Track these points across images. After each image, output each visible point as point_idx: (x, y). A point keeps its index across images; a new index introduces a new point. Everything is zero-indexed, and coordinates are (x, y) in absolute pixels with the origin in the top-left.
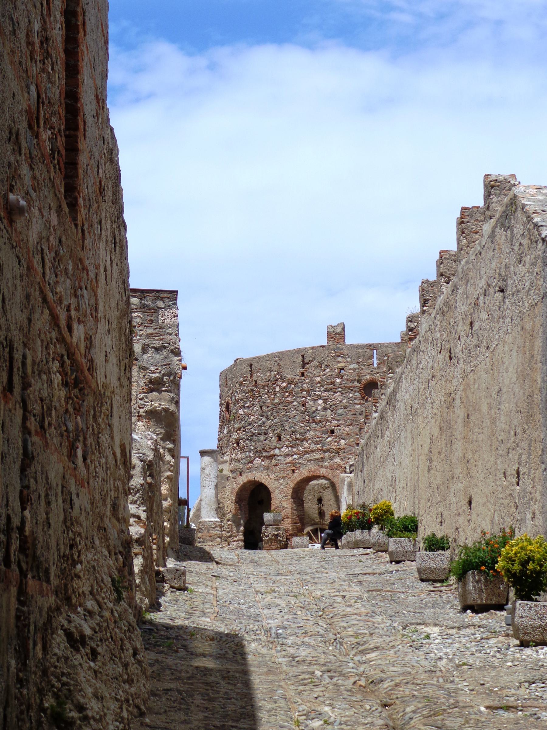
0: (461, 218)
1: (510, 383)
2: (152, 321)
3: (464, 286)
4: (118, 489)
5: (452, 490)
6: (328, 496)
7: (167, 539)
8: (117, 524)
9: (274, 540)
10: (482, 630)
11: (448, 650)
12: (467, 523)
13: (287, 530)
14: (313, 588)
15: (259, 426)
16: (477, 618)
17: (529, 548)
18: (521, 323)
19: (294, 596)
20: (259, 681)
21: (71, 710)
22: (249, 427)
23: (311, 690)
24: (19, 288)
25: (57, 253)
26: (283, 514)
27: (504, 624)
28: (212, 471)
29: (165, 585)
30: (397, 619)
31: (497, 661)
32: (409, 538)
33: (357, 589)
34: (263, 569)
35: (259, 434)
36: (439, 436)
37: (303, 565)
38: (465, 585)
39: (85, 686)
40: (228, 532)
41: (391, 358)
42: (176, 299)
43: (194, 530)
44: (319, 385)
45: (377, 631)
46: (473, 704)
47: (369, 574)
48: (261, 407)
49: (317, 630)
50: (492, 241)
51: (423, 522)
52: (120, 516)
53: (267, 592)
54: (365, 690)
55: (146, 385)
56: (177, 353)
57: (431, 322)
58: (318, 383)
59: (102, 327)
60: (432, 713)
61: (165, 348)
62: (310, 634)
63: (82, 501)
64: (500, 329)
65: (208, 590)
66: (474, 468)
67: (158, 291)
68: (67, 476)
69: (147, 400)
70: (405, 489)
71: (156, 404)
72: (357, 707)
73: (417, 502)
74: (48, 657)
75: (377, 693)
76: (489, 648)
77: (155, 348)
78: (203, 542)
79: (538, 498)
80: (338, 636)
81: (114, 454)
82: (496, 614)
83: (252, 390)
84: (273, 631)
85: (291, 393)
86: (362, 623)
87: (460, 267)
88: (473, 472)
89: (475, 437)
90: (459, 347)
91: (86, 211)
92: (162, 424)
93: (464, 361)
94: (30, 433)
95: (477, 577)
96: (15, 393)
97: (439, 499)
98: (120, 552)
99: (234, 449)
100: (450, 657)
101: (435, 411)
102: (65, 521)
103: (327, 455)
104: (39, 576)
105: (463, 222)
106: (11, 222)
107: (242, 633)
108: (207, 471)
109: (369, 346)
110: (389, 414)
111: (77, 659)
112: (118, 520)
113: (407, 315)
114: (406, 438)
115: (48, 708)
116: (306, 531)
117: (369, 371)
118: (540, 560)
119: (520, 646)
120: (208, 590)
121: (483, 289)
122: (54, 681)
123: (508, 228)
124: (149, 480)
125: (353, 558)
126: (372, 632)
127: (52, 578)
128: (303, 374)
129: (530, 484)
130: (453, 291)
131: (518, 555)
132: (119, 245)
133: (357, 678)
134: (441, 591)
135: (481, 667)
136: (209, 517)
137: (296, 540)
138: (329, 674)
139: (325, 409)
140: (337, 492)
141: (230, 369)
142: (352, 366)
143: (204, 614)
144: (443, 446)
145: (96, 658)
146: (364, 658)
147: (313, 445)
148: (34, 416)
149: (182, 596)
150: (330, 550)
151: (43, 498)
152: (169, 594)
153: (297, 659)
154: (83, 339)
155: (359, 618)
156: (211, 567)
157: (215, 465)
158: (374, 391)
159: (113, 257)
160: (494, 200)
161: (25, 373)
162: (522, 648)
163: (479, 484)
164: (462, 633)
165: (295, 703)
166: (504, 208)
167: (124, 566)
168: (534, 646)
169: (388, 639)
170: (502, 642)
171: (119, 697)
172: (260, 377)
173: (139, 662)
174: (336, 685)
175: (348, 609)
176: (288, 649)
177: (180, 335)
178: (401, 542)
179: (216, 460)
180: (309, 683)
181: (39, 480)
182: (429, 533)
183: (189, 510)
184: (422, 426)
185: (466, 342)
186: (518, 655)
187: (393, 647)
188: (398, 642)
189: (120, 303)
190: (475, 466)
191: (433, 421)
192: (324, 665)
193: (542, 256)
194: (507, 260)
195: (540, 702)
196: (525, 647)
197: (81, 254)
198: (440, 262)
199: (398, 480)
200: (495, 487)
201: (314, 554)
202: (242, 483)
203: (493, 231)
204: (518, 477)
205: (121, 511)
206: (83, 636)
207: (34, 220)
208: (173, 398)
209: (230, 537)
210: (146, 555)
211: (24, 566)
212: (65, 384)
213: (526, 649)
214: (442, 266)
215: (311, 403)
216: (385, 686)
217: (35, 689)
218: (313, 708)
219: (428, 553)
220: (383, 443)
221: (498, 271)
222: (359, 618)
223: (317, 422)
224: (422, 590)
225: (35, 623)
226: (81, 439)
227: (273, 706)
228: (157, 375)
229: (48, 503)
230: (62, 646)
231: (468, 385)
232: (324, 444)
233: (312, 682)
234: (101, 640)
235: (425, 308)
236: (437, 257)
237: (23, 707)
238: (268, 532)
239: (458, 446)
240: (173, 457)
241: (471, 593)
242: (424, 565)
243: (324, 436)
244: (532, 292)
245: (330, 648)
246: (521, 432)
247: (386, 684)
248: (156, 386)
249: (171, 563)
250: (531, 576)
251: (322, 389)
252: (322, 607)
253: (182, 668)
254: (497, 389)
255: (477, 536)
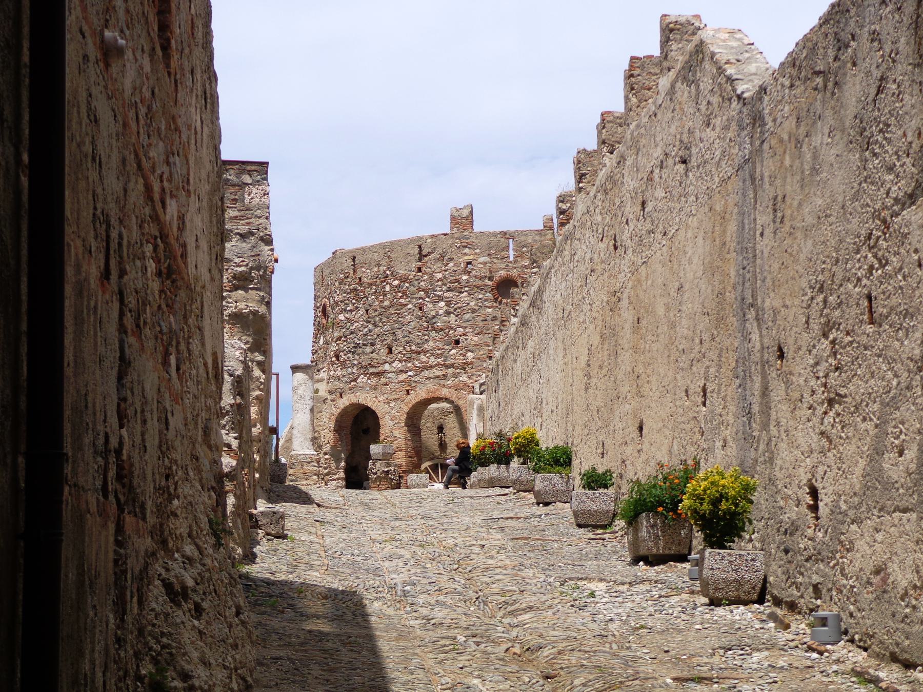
0: (630, 70)
1: (695, 278)
2: (236, 200)
3: (634, 157)
4: (210, 409)
5: (617, 413)
6: (451, 423)
7: (257, 475)
8: (209, 452)
9: (384, 478)
10: (660, 586)
11: (620, 611)
12: (636, 454)
13: (400, 466)
14: (443, 535)
15: (365, 335)
16: (652, 572)
17: (722, 482)
18: (709, 202)
19: (420, 546)
20: (387, 646)
21: (173, 679)
22: (351, 336)
23: (454, 658)
24: (115, 151)
25: (149, 108)
26: (395, 445)
27: (687, 579)
28: (305, 391)
29: (260, 531)
30: (551, 573)
31: (683, 623)
32: (560, 474)
33: (499, 536)
34: (376, 513)
35: (364, 345)
36: (600, 346)
37: (426, 508)
38: (636, 531)
39: (190, 648)
40: (326, 468)
41: (539, 248)
42: (266, 173)
43: (285, 465)
44: (440, 283)
45: (529, 587)
46: (657, 676)
47: (512, 518)
48: (367, 311)
49: (453, 586)
50: (671, 99)
51: (579, 454)
52: (212, 443)
53: (386, 541)
54: (520, 659)
55: (229, 282)
56: (268, 240)
57: (589, 203)
58: (439, 280)
59: (194, 204)
60: (607, 686)
61: (253, 234)
62: (445, 591)
63: (175, 422)
64: (681, 210)
65: (313, 538)
66: (646, 385)
67: (243, 163)
68: (162, 390)
69: (230, 300)
70: (555, 413)
71: (241, 305)
72: (512, 679)
73: (571, 429)
74: (144, 612)
75: (535, 663)
76: (671, 607)
77: (241, 235)
78: (296, 481)
79: (731, 422)
80: (480, 593)
81: (205, 364)
82: (676, 567)
83: (355, 290)
84: (399, 587)
85: (404, 293)
86: (508, 578)
87: (629, 132)
88: (645, 390)
89: (647, 346)
90: (627, 234)
91: (178, 56)
92: (249, 331)
93: (634, 251)
94: (126, 332)
95: (652, 520)
96: (112, 281)
97: (599, 424)
98: (213, 488)
99: (332, 363)
100: (624, 618)
101: (594, 314)
102: (160, 446)
103: (450, 371)
104: (135, 512)
105: (632, 76)
106: (107, 65)
107: (361, 590)
108: (300, 392)
109: (504, 234)
110: (534, 318)
111: (179, 615)
112: (210, 447)
113: (558, 194)
114: (556, 349)
115: (145, 676)
116: (423, 467)
117: (503, 266)
118: (735, 498)
119: (709, 605)
120: (313, 538)
121: (659, 160)
122: (152, 643)
123: (693, 82)
124: (239, 400)
125: (488, 500)
126: (522, 589)
127: (148, 515)
128: (419, 270)
129: (720, 404)
130: (619, 163)
131: (708, 492)
132: (210, 101)
133: (510, 644)
134: (604, 539)
135: (664, 631)
136: (302, 448)
137: (412, 478)
138: (475, 639)
139: (448, 313)
140: (462, 418)
141: (327, 264)
142: (482, 259)
143: (311, 567)
144: (606, 358)
145: (201, 615)
146: (515, 621)
147: (432, 359)
148: (130, 311)
149: (283, 545)
150: (456, 489)
151: (139, 415)
152: (264, 542)
153: (433, 622)
154: (175, 218)
155: (505, 572)
156: (312, 511)
157: (310, 383)
158: (513, 290)
159: (204, 116)
160: (674, 47)
161: (121, 257)
162: (712, 607)
163: (653, 405)
164: (635, 590)
165: (436, 674)
166: (687, 57)
167: (217, 506)
168: (728, 605)
169: (544, 598)
170: (686, 601)
171: (227, 664)
172: (367, 274)
173: (243, 623)
174: (485, 652)
175: (490, 561)
176: (420, 609)
177: (271, 218)
178: (550, 480)
179: (311, 378)
180: (451, 650)
181: (136, 392)
182: (586, 467)
183: (278, 439)
184: (577, 334)
185: (636, 226)
186: (708, 616)
187: (550, 607)
188: (557, 601)
189: (211, 175)
190: (648, 382)
191: (592, 326)
192: (467, 629)
193: (737, 117)
194: (691, 123)
195: (740, 674)
196: (716, 606)
197: (174, 111)
198: (602, 125)
199: (544, 402)
200: (674, 409)
201: (437, 492)
202: (342, 407)
203: (673, 86)
204: (705, 395)
205: (213, 436)
206: (185, 588)
207: (128, 65)
208: (263, 298)
209: (327, 474)
210: (238, 493)
211: (122, 499)
212: (159, 274)
213: (718, 609)
214: (604, 131)
215: (430, 306)
216: (545, 654)
217: (131, 652)
218: (459, 681)
219: (587, 491)
220: (524, 355)
221: (678, 137)
222: (505, 572)
223: (438, 330)
224: (580, 538)
225: (132, 570)
226: (174, 343)
227: (409, 678)
228: (243, 269)
229: (144, 422)
230: (160, 599)
231: (639, 281)
232: (446, 357)
233: (454, 649)
234: (204, 593)
235: (581, 185)
236: (598, 120)
237: (121, 673)
238: (377, 468)
239: (626, 358)
240: (264, 372)
241: (644, 541)
242: (582, 506)
243: (446, 347)
244: (723, 163)
245: (472, 609)
246: (708, 340)
247: (546, 652)
248: (241, 283)
249: (262, 506)
250: (723, 518)
251: (444, 288)
252: (457, 559)
253: (292, 632)
254: (677, 285)
255: (651, 470)
